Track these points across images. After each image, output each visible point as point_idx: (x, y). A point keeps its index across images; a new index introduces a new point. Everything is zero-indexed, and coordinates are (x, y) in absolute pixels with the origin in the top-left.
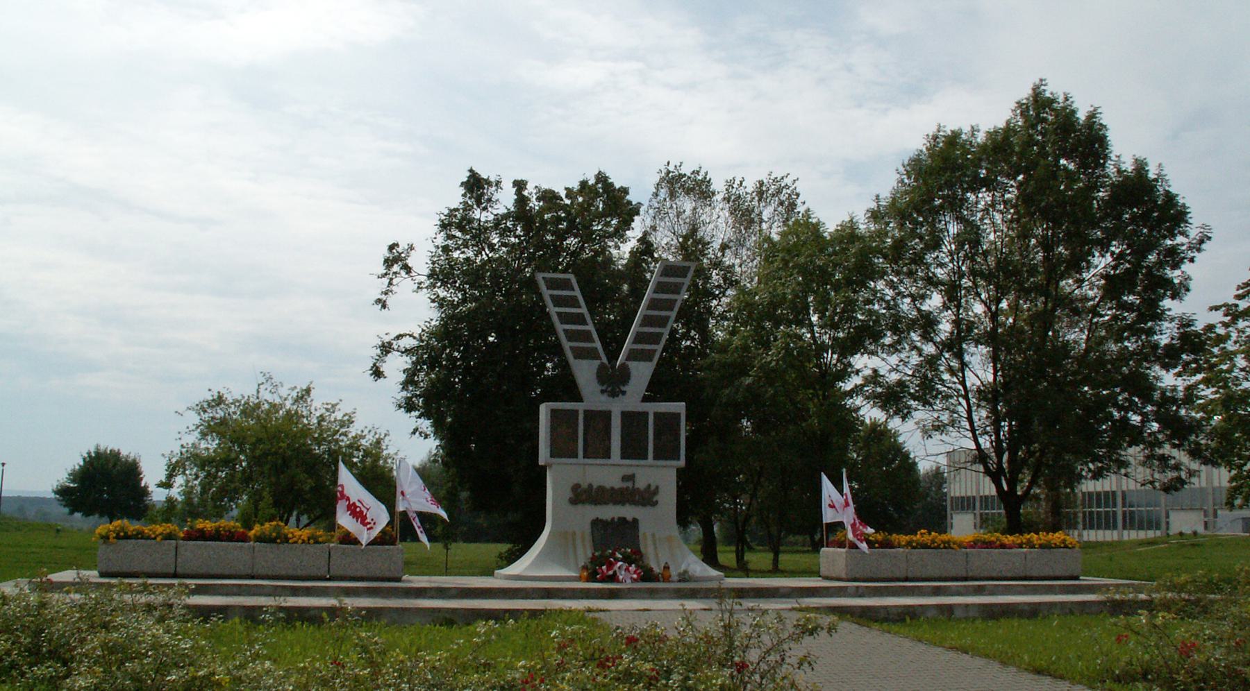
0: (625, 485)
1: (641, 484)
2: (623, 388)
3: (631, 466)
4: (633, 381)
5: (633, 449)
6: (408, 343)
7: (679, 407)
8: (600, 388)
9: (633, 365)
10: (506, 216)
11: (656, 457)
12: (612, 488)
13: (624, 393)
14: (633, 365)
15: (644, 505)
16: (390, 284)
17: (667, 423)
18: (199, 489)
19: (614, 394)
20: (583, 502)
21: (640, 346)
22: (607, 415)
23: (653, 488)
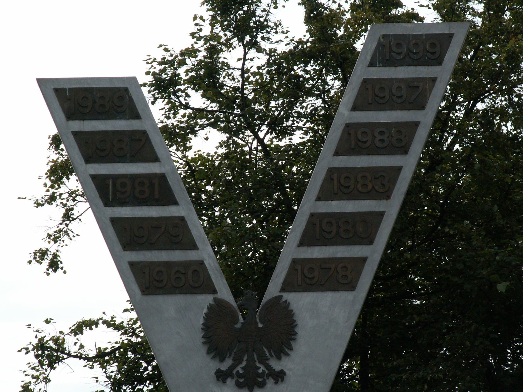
2: (276, 365)
4: (301, 346)
6: (106, 338)
8: (214, 365)
9: (300, 302)
10: (299, 54)
13: (279, 376)
14: (300, 302)
16: (68, 216)
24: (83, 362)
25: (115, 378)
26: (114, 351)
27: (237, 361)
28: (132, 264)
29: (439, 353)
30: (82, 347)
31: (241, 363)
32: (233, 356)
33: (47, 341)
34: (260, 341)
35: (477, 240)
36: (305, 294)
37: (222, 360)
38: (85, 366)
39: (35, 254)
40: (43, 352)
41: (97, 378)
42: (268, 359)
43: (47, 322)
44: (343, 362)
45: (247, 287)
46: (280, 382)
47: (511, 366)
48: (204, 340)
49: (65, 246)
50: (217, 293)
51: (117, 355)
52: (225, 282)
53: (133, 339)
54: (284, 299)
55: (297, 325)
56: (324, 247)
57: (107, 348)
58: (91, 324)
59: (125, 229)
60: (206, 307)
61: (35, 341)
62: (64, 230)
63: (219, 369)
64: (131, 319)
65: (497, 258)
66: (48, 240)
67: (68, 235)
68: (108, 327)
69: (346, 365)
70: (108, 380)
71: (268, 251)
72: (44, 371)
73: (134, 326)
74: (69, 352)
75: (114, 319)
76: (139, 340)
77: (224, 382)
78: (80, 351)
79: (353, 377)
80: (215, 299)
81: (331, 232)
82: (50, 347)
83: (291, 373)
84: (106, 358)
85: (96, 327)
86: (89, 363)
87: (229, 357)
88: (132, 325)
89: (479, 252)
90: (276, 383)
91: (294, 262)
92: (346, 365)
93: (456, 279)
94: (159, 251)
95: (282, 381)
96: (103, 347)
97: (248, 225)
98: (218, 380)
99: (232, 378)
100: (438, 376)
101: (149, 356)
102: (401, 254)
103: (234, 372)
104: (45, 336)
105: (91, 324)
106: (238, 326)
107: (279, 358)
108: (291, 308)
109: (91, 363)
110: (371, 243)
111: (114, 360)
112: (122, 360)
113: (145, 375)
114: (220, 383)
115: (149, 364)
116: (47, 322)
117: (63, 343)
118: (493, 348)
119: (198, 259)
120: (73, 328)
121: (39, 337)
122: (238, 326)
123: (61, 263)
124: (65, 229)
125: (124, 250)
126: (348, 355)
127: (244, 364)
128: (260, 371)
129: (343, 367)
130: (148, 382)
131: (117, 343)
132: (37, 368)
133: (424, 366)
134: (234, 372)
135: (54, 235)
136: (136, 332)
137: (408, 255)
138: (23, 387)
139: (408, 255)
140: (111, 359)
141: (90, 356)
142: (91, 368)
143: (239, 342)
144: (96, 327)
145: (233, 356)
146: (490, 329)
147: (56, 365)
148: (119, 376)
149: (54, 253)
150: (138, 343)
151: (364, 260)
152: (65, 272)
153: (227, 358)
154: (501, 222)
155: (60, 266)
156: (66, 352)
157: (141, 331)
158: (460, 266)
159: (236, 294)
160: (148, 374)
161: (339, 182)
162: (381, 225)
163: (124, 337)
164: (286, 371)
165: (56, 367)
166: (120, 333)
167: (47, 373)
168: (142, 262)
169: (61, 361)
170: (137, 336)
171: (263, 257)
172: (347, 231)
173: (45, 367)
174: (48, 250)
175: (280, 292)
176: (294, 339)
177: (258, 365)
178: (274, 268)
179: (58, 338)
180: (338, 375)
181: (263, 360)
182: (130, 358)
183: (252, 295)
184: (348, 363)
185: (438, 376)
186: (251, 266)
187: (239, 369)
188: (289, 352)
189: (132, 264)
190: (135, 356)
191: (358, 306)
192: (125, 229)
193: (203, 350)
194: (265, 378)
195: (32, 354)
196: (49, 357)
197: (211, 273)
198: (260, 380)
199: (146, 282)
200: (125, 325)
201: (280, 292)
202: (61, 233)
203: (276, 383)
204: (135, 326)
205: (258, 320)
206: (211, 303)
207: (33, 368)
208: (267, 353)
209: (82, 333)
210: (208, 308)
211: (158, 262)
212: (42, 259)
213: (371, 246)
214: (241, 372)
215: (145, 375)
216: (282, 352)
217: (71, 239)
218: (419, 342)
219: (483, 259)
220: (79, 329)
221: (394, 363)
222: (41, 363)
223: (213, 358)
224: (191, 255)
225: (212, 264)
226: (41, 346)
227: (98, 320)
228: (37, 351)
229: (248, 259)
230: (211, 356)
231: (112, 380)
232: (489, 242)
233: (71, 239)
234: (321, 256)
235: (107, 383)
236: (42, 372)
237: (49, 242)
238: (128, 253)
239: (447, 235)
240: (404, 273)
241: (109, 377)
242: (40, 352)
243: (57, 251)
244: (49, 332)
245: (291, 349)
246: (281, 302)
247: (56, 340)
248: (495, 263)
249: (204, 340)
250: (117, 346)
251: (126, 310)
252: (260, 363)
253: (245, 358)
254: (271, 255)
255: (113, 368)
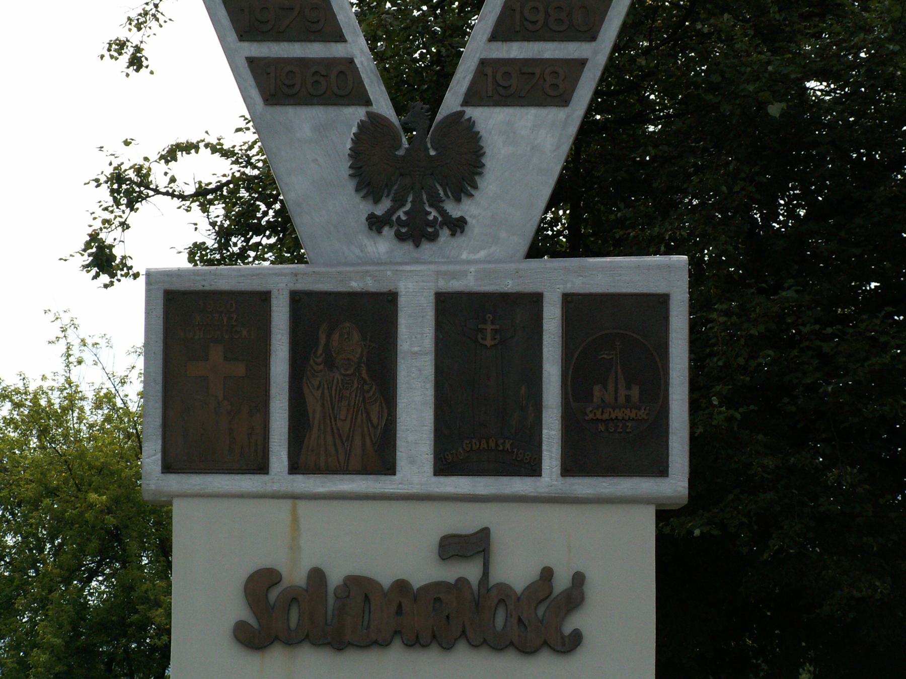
0: (450, 573)
1: (514, 568)
2: (454, 210)
3: (478, 500)
4: (491, 183)
5: (484, 433)
7: (665, 274)
8: (365, 208)
9: (491, 121)
11: (572, 466)
12: (401, 586)
13: (458, 226)
14: (491, 121)
15: (527, 650)
17: (612, 335)
18: (741, 410)
19: (417, 232)
20: (291, 640)
21: (516, 50)
22: (376, 313)
23: (561, 582)
24: (177, 202)
25: (221, 226)
26: (220, 188)
27: (399, 202)
28: (251, 61)
29: (681, 202)
30: (173, 180)
31: (403, 205)
32: (392, 195)
33: (126, 170)
34: (432, 174)
35: (742, 41)
36: (497, 110)
37: (377, 201)
38: (179, 208)
39: (110, 45)
40: (120, 187)
41: (196, 224)
42: (442, 201)
43: (127, 143)
44: (546, 212)
45: (413, 99)
46: (458, 233)
47: (784, 224)
48: (351, 172)
49: (152, 36)
50: (372, 105)
51: (225, 193)
52: (384, 89)
53: (249, 171)
54: (466, 117)
55: (484, 153)
56: (526, 43)
57: (210, 183)
58: (189, 147)
59: (242, 10)
60: (356, 125)
61: (109, 171)
62: (151, 13)
63: (373, 214)
64: (245, 143)
65: (770, 68)
66: (128, 26)
67: (157, 20)
68: (213, 153)
69: (549, 216)
70: (211, 228)
71: (443, 50)
72: (121, 214)
73: (248, 152)
74: (157, 186)
75: (221, 141)
76: (256, 172)
77: (379, 231)
78: (171, 185)
79: (560, 233)
80: (369, 114)
81: (537, 21)
82: (130, 179)
83: (474, 221)
84: (210, 197)
85: (197, 152)
86: (184, 202)
87: (388, 195)
88: (246, 150)
89: (744, 59)
90: (453, 235)
91: (483, 62)
92: (549, 216)
93: (709, 97)
94: (290, 44)
95: (462, 232)
96: (205, 181)
97: (416, 13)
98: (370, 229)
99: (391, 227)
100: (680, 234)
101: (271, 195)
102: (633, 59)
103: (394, 218)
104: (122, 163)
105: (189, 147)
106: (401, 152)
107: (458, 200)
108: (478, 128)
109: (188, 203)
110: (593, 38)
111: (220, 200)
112: (230, 201)
113: (263, 222)
114: (374, 234)
115: (269, 206)
116: (127, 143)
117: (148, 175)
118: (759, 197)
119: (346, 56)
120: (163, 153)
121: (115, 165)
122: (401, 152)
123: (147, 59)
124: (153, 11)
125: (240, 40)
126: (553, 202)
127: (408, 207)
128: (431, 218)
129: (546, 217)
130: (268, 233)
131: (224, 175)
132: (110, 209)
133: (660, 219)
134: (394, 218)
135: (138, 20)
136: (253, 161)
137: (642, 61)
138: (90, 235)
139: (642, 61)
140: (216, 199)
141: (186, 194)
142: (187, 211)
143: (402, 175)
144: (197, 152)
145: (392, 195)
146: (757, 168)
147: (137, 205)
148: (228, 222)
149: (137, 46)
150: (255, 177)
151: (582, 63)
152: (152, 73)
153: (384, 198)
154: (777, 16)
155: (145, 63)
156: (151, 186)
157: (259, 160)
158: (716, 78)
159: (399, 109)
160: (268, 222)
161: (522, 12)
162: (609, 14)
163: (236, 167)
164: (467, 218)
165: (137, 209)
166: (230, 161)
167: (124, 216)
168: (265, 58)
169: (145, 199)
170: (254, 167)
171: (437, 59)
172: (559, 21)
173: (123, 207)
174: (128, 41)
175: (462, 105)
176: (480, 174)
177: (429, 209)
178: (452, 74)
179: (141, 167)
180: (540, 230)
181: (436, 203)
182: (242, 197)
183: (422, 108)
184: (552, 213)
185: (680, 234)
186: (418, 72)
187: (401, 214)
188: (473, 192)
189: (251, 61)
190: (250, 195)
191: (573, 129)
192: (242, 10)
193: (351, 185)
194: (438, 227)
195: (105, 188)
196: (128, 193)
197: (363, 75)
198: (430, 230)
199: (273, 86)
200: (237, 150)
201: (462, 105)
202: (148, 17)
203: (453, 235)
204: (251, 153)
205: (429, 145)
206: (363, 119)
207: (106, 209)
208: (441, 192)
209: (176, 160)
210: (359, 126)
211: (288, 59)
212: (120, 54)
213: (594, 44)
214: (404, 218)
215: (263, 222)
216: (462, 191)
217: (161, 26)
218: (655, 185)
219: (749, 69)
220: (170, 156)
221: (619, 214)
222: (117, 203)
223: (364, 197)
224: (336, 50)
225: (365, 64)
226: (117, 177)
227: (198, 142)
228: (112, 184)
229: (416, 61)
230: (362, 194)
231: (217, 228)
232: (758, 45)
233: (161, 26)
234: (522, 56)
235: (210, 233)
236: (117, 214)
237: (130, 30)
238: (245, 45)
239: (699, 33)
240: (635, 88)
241: (213, 224)
242: (115, 186)
243: (141, 42)
244: (129, 158)
245: (475, 187)
246: (463, 120)
247: (138, 170)
248: (766, 75)
249: (351, 172)
250: (224, 180)
251: (239, 130)
252: (431, 206)
253: (410, 199)
254: (448, 56)
255: (218, 210)
